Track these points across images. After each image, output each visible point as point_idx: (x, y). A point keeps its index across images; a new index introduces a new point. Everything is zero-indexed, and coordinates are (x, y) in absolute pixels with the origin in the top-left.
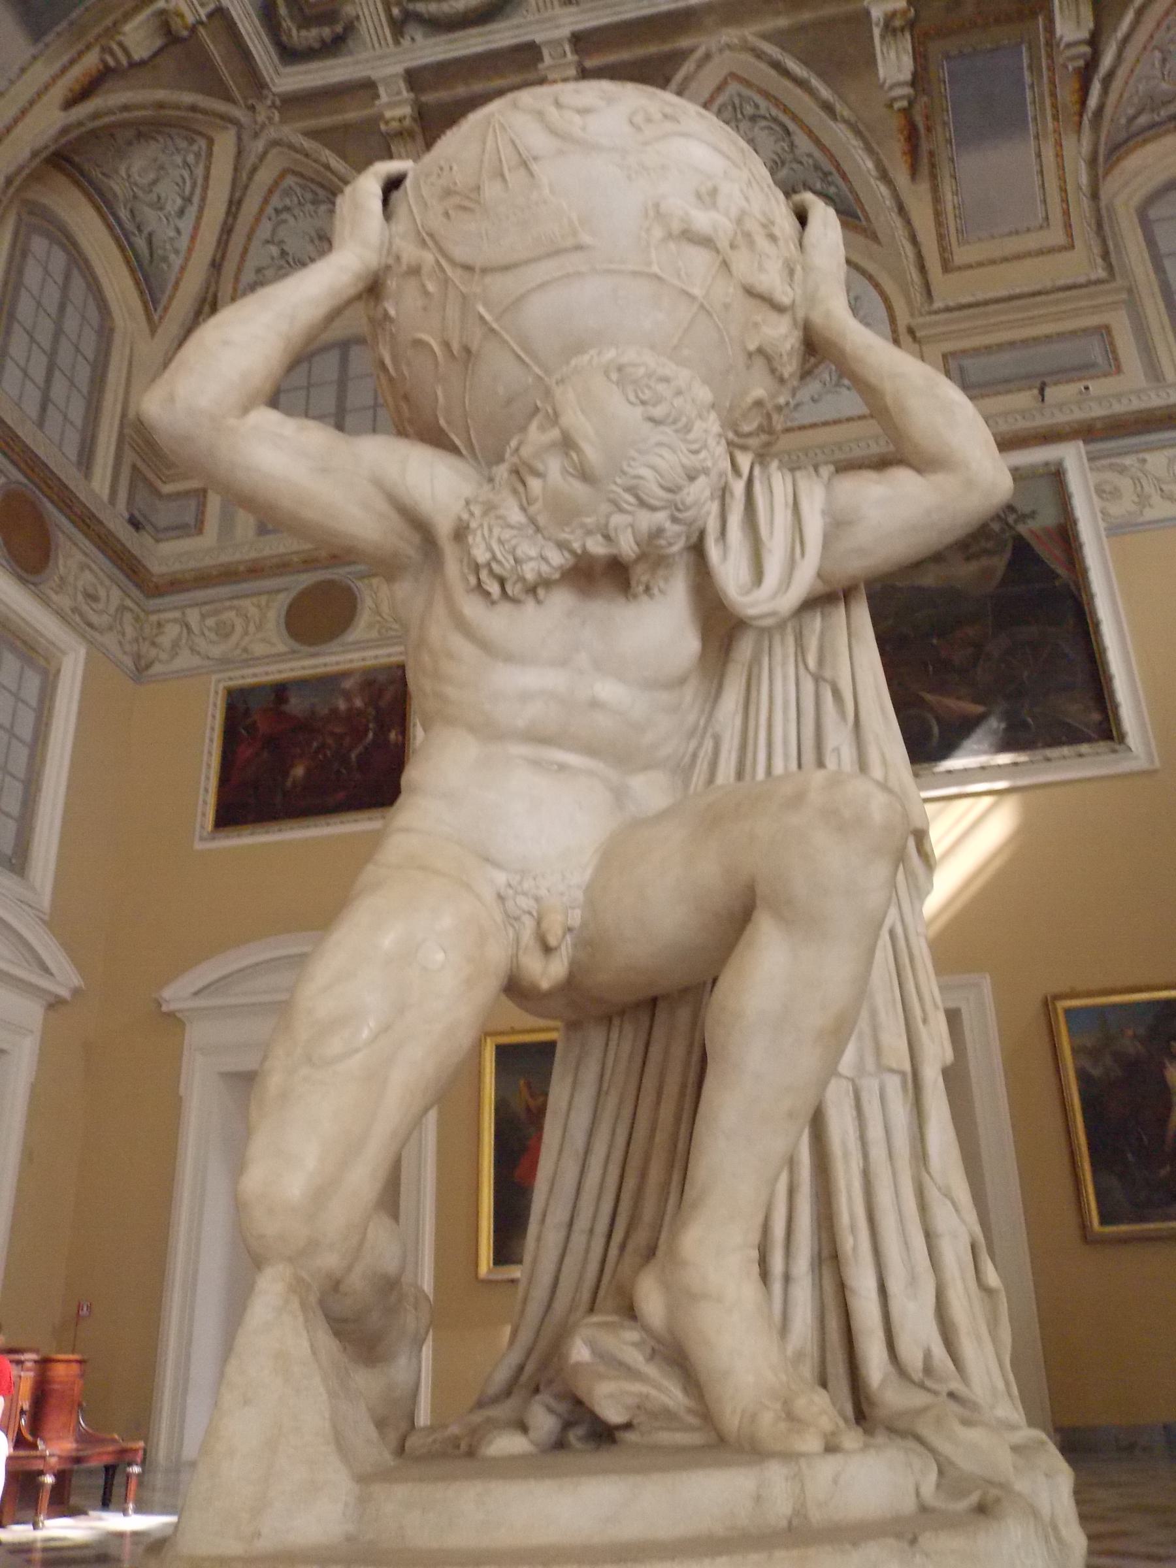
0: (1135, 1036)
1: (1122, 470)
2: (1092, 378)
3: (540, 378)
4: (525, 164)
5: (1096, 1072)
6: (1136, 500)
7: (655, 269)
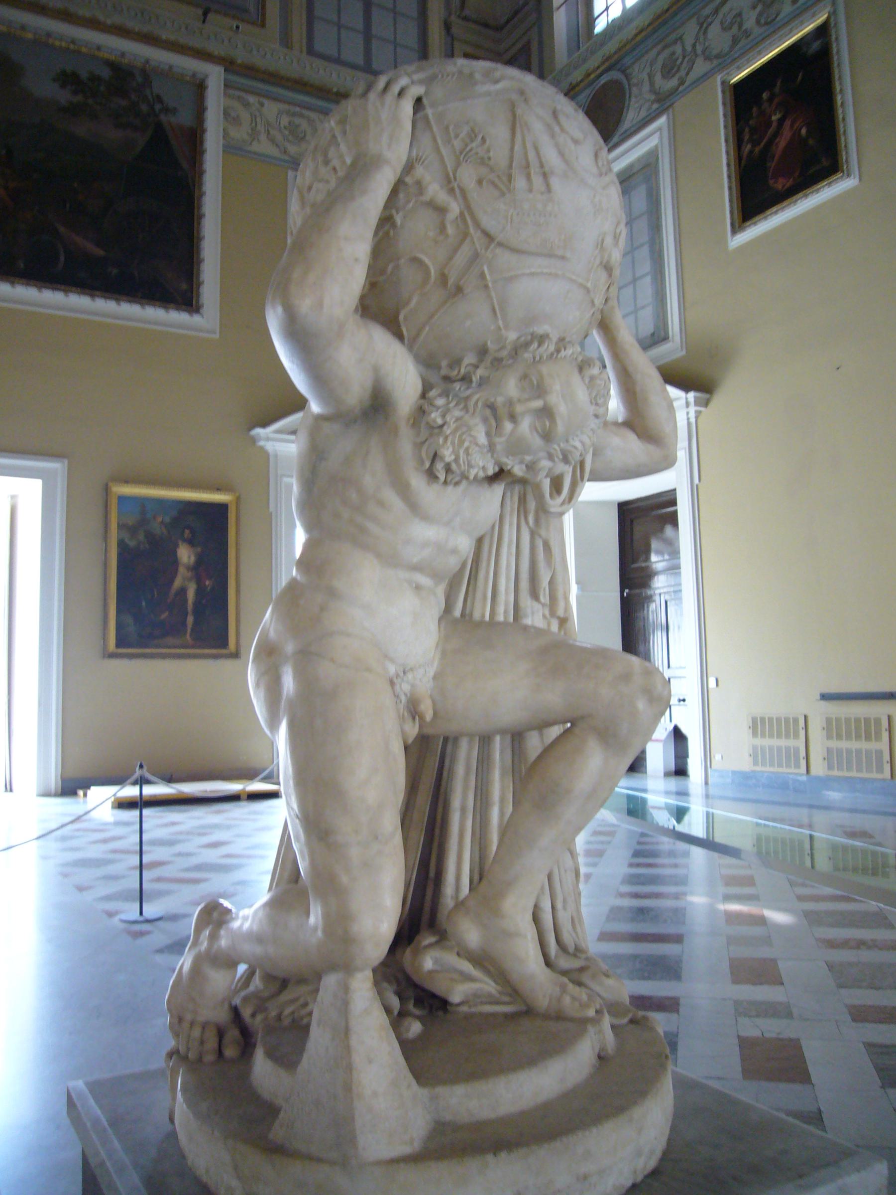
0: (162, 522)
1: (247, 105)
2: (243, 21)
3: (499, 328)
4: (545, 176)
5: (132, 543)
6: (250, 131)
7: (589, 285)
